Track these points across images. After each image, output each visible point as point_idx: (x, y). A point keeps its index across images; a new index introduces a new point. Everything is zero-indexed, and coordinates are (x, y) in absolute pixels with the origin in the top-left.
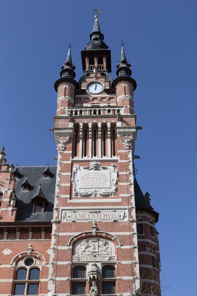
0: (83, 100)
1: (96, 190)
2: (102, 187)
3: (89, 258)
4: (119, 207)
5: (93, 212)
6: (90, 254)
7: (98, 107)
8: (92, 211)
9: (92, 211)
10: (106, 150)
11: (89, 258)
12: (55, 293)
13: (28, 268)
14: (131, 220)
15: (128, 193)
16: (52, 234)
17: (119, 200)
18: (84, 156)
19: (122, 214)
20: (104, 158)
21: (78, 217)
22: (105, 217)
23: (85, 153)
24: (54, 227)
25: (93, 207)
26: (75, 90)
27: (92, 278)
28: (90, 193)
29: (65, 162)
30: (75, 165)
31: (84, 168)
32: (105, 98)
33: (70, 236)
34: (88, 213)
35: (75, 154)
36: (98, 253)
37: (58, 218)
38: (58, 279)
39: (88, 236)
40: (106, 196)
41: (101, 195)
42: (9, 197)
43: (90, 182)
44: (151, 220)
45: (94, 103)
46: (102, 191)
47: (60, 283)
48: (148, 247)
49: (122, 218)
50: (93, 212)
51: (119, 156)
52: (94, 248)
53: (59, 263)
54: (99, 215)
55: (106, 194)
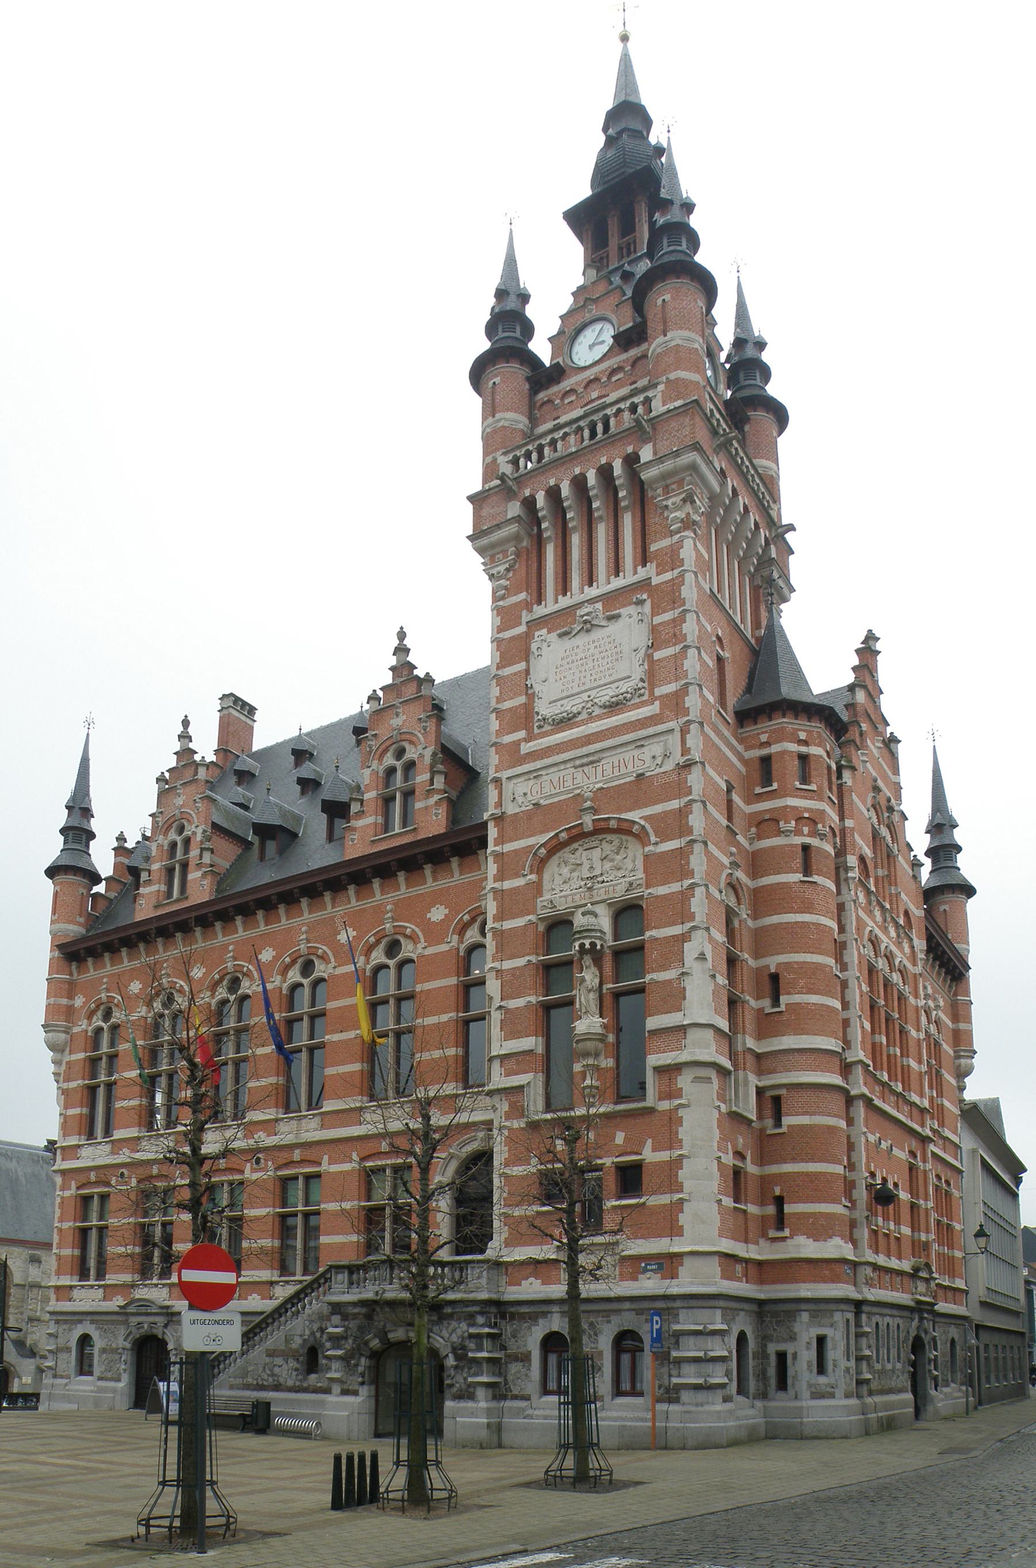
1: (593, 693)
2: (608, 679)
4: (651, 731)
5: (582, 765)
8: (578, 762)
9: (578, 762)
10: (612, 555)
13: (232, 998)
16: (489, 851)
17: (655, 708)
18: (560, 597)
20: (617, 583)
21: (548, 789)
22: (616, 769)
23: (564, 587)
24: (492, 832)
25: (585, 750)
27: (587, 946)
28: (575, 710)
31: (560, 636)
33: (527, 850)
35: (540, 599)
36: (600, 879)
37: (499, 804)
38: (507, 965)
39: (578, 836)
40: (614, 707)
42: (428, 767)
45: (592, 401)
46: (606, 695)
47: (513, 975)
49: (659, 761)
50: (582, 765)
54: (599, 770)
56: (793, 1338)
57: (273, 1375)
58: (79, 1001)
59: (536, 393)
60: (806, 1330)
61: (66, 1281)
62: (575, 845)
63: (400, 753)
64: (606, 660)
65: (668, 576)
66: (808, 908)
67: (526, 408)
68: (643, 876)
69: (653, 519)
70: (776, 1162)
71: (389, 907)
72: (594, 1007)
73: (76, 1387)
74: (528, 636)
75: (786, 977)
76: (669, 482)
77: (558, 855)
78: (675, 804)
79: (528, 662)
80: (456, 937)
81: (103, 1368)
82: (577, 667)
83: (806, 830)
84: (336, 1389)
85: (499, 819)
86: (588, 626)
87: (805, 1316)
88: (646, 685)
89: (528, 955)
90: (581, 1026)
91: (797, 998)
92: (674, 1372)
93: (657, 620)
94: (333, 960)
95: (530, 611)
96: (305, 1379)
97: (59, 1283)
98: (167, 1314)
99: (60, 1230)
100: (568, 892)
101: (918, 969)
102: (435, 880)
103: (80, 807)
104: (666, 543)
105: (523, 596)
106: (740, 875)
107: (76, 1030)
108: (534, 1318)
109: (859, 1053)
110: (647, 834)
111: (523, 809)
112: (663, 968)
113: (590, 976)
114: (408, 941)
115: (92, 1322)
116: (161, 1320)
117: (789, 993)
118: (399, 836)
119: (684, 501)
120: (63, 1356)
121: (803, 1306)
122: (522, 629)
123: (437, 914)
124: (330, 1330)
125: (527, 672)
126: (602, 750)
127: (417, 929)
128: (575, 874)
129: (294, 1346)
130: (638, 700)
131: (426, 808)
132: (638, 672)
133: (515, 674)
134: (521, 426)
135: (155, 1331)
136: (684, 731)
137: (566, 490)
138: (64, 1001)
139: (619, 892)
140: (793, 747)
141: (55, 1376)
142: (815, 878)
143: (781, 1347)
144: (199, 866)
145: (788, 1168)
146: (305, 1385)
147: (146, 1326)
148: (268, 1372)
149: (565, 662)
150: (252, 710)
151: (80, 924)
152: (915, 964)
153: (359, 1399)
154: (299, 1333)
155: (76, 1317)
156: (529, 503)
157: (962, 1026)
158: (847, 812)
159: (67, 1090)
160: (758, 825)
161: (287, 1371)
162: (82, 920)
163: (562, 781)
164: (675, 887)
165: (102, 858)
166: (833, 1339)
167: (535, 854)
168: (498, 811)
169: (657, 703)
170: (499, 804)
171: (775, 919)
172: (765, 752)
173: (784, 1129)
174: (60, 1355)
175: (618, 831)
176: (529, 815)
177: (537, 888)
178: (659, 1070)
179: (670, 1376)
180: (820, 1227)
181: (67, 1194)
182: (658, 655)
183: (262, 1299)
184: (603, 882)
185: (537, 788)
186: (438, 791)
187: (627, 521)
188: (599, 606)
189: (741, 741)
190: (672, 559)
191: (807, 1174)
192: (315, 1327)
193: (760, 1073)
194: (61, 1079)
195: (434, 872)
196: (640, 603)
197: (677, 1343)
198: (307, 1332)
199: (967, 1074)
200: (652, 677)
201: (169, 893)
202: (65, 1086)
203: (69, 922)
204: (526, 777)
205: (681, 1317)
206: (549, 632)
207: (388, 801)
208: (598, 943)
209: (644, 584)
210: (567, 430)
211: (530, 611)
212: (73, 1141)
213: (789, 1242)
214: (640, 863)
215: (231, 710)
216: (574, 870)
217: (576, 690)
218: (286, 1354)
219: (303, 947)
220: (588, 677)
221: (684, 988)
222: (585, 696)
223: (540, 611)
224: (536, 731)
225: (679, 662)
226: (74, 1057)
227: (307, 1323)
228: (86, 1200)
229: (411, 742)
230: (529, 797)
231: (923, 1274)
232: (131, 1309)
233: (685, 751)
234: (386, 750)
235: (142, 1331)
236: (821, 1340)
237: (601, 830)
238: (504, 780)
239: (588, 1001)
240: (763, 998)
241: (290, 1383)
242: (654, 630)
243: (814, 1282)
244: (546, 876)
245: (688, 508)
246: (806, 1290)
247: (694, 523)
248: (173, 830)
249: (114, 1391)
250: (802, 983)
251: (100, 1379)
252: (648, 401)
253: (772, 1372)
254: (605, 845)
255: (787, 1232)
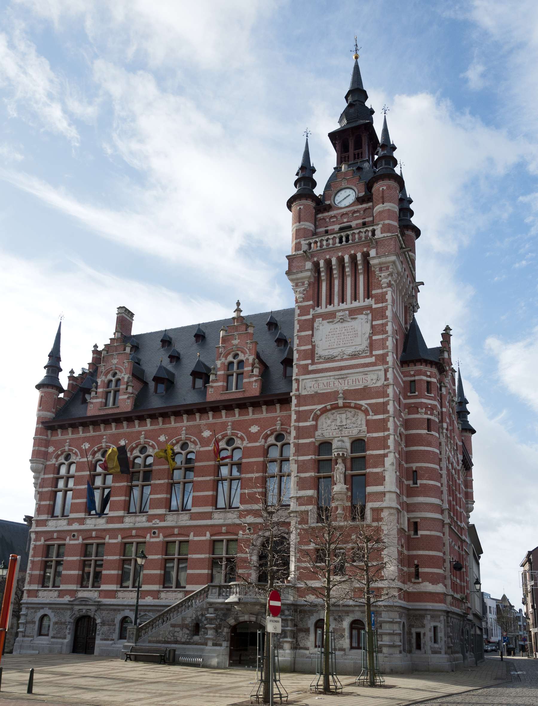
0: (328, 220)
1: (344, 349)
2: (351, 344)
3: (335, 433)
5: (339, 379)
6: (337, 428)
7: (350, 228)
8: (336, 377)
10: (353, 291)
11: (335, 433)
12: (298, 473)
14: (385, 383)
15: (383, 349)
17: (373, 359)
18: (328, 306)
19: (375, 377)
20: (356, 304)
22: (354, 382)
23: (330, 301)
24: (294, 401)
26: (314, 208)
27: (341, 455)
28: (335, 354)
29: (304, 318)
30: (317, 320)
31: (328, 322)
32: (357, 211)
33: (312, 410)
34: (334, 380)
35: (318, 304)
36: (345, 427)
37: (298, 390)
38: (301, 458)
40: (354, 356)
41: (349, 355)
43: (336, 340)
44: (429, 373)
45: (344, 223)
46: (350, 351)
48: (422, 409)
49: (374, 381)
50: (339, 379)
51: (373, 300)
52: (341, 422)
53: (301, 441)
55: (356, 353)
56: (423, 626)
57: (174, 636)
58: (51, 449)
59: (318, 214)
60: (429, 624)
61: (35, 587)
62: (333, 411)
63: (236, 356)
64: (350, 336)
65: (380, 305)
66: (429, 445)
67: (313, 221)
68: (366, 428)
69: (373, 281)
70: (415, 550)
71: (229, 424)
72: (342, 480)
73: (38, 642)
74: (313, 320)
75: (420, 472)
76: (382, 266)
77: (325, 414)
78: (381, 400)
79: (313, 331)
80: (263, 440)
81: (55, 632)
82: (336, 337)
83: (429, 412)
84: (210, 643)
85: (298, 397)
86: (342, 320)
87: (429, 617)
88: (368, 349)
89: (311, 455)
90: (336, 488)
91: (425, 482)
92: (379, 639)
93: (374, 323)
94: (199, 444)
95: (314, 309)
96: (191, 639)
97: (31, 588)
98: (98, 605)
99: (33, 562)
100: (330, 431)
101: (459, 468)
102: (253, 414)
103: (55, 356)
104: (379, 291)
105: (311, 303)
106: (402, 430)
107: (48, 463)
108: (347, 613)
109: (446, 506)
110: (368, 411)
111: (309, 393)
112: (375, 467)
113: (340, 467)
114: (238, 439)
115: (50, 608)
116: (93, 608)
117: (421, 479)
118: (234, 393)
119: (389, 275)
120: (30, 626)
121: (428, 612)
122: (310, 317)
123: (254, 429)
124: (208, 615)
125: (313, 335)
126: (348, 374)
127: (243, 435)
128: (333, 423)
129: (186, 622)
130: (365, 355)
131: (249, 382)
132: (366, 343)
133: (306, 335)
134: (311, 229)
135: (89, 614)
136: (386, 371)
137: (334, 261)
138: (43, 449)
139: (354, 432)
140: (425, 378)
141: (24, 636)
142: (433, 433)
143: (418, 630)
144: (125, 393)
145: (421, 552)
146: (192, 641)
147: (84, 611)
148: (171, 635)
149: (330, 334)
150: (132, 315)
151: (53, 412)
152: (458, 465)
153: (223, 648)
154: (189, 616)
155: (40, 606)
156: (316, 265)
157: (469, 490)
158: (443, 405)
159: (41, 492)
160: (409, 408)
161: (182, 635)
162: (54, 410)
163: (328, 384)
164: (381, 434)
165: (64, 381)
166: (440, 627)
167: (315, 413)
168: (297, 393)
169: (374, 358)
170: (298, 390)
171: (416, 448)
172: (413, 379)
173: (419, 536)
174: (28, 625)
175: (355, 408)
176: (312, 396)
177: (315, 427)
178: (373, 510)
179: (377, 641)
180: (434, 579)
181: (38, 543)
182: (374, 338)
183: (153, 599)
184: (347, 428)
185: (316, 385)
186: (256, 376)
187: (361, 279)
188: (347, 312)
189: (402, 373)
190: (382, 298)
191: (429, 556)
192: (199, 613)
193: (408, 512)
194: (38, 486)
195: (253, 411)
196: (367, 314)
197: (381, 626)
198: (194, 616)
199: (471, 511)
200: (372, 345)
201: (106, 404)
202: (41, 490)
203: (48, 411)
204: (311, 380)
205: (383, 615)
206: (323, 320)
207: (228, 376)
208: (345, 454)
209: (369, 308)
210: (335, 235)
211: (314, 309)
212: (44, 517)
213: (422, 584)
214: (364, 422)
215: (123, 314)
216: (333, 422)
217: (335, 346)
218: (183, 626)
219: (183, 437)
220: (342, 342)
221: (385, 476)
222: (340, 350)
223: (319, 310)
224: (316, 361)
225: (384, 342)
226: (46, 476)
227: (194, 612)
228: (49, 547)
229: (242, 352)
230: (312, 388)
231: (464, 601)
232: (76, 602)
233: (386, 379)
234: (229, 354)
235: (81, 613)
236: (435, 628)
237: (346, 406)
238: (300, 380)
239: (340, 477)
240: (409, 480)
241: (183, 640)
242: (372, 327)
243: (432, 602)
244: (319, 423)
245: (390, 278)
246: (429, 605)
247: (392, 285)
248: (110, 374)
249: (62, 644)
250: (427, 475)
251: (53, 637)
252: (373, 232)
253: (414, 641)
254: (347, 413)
255: (420, 580)
